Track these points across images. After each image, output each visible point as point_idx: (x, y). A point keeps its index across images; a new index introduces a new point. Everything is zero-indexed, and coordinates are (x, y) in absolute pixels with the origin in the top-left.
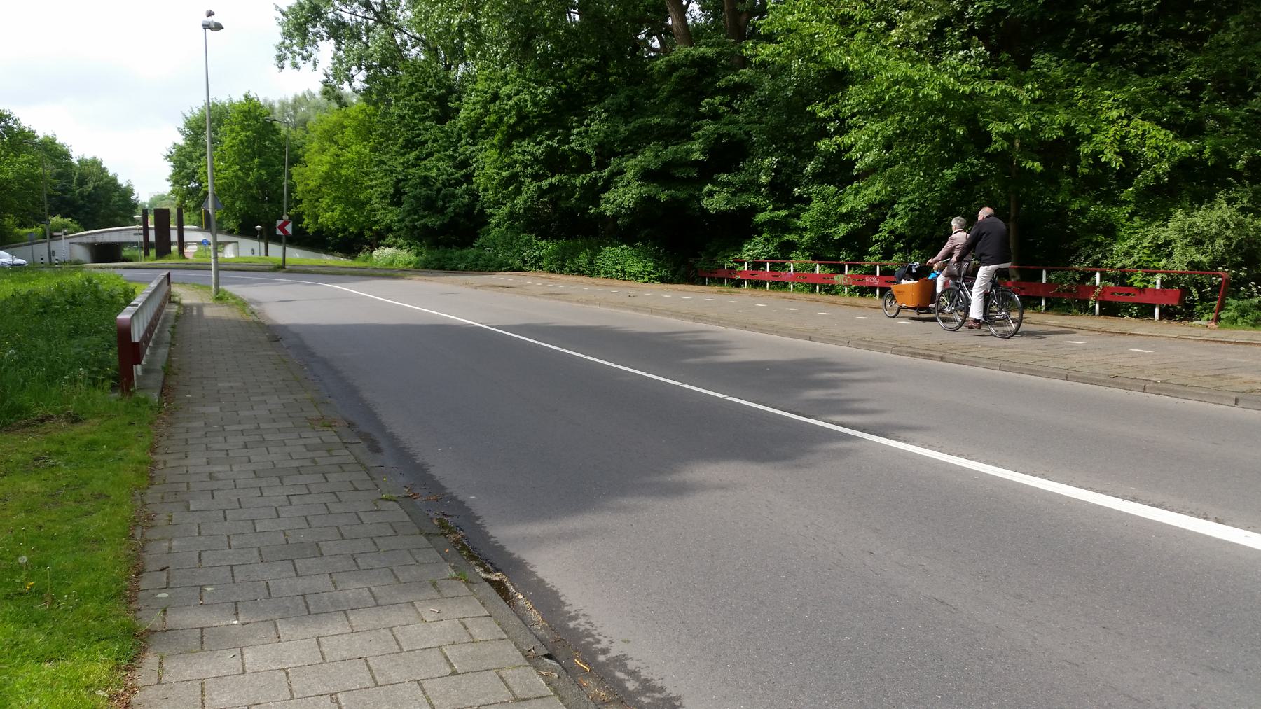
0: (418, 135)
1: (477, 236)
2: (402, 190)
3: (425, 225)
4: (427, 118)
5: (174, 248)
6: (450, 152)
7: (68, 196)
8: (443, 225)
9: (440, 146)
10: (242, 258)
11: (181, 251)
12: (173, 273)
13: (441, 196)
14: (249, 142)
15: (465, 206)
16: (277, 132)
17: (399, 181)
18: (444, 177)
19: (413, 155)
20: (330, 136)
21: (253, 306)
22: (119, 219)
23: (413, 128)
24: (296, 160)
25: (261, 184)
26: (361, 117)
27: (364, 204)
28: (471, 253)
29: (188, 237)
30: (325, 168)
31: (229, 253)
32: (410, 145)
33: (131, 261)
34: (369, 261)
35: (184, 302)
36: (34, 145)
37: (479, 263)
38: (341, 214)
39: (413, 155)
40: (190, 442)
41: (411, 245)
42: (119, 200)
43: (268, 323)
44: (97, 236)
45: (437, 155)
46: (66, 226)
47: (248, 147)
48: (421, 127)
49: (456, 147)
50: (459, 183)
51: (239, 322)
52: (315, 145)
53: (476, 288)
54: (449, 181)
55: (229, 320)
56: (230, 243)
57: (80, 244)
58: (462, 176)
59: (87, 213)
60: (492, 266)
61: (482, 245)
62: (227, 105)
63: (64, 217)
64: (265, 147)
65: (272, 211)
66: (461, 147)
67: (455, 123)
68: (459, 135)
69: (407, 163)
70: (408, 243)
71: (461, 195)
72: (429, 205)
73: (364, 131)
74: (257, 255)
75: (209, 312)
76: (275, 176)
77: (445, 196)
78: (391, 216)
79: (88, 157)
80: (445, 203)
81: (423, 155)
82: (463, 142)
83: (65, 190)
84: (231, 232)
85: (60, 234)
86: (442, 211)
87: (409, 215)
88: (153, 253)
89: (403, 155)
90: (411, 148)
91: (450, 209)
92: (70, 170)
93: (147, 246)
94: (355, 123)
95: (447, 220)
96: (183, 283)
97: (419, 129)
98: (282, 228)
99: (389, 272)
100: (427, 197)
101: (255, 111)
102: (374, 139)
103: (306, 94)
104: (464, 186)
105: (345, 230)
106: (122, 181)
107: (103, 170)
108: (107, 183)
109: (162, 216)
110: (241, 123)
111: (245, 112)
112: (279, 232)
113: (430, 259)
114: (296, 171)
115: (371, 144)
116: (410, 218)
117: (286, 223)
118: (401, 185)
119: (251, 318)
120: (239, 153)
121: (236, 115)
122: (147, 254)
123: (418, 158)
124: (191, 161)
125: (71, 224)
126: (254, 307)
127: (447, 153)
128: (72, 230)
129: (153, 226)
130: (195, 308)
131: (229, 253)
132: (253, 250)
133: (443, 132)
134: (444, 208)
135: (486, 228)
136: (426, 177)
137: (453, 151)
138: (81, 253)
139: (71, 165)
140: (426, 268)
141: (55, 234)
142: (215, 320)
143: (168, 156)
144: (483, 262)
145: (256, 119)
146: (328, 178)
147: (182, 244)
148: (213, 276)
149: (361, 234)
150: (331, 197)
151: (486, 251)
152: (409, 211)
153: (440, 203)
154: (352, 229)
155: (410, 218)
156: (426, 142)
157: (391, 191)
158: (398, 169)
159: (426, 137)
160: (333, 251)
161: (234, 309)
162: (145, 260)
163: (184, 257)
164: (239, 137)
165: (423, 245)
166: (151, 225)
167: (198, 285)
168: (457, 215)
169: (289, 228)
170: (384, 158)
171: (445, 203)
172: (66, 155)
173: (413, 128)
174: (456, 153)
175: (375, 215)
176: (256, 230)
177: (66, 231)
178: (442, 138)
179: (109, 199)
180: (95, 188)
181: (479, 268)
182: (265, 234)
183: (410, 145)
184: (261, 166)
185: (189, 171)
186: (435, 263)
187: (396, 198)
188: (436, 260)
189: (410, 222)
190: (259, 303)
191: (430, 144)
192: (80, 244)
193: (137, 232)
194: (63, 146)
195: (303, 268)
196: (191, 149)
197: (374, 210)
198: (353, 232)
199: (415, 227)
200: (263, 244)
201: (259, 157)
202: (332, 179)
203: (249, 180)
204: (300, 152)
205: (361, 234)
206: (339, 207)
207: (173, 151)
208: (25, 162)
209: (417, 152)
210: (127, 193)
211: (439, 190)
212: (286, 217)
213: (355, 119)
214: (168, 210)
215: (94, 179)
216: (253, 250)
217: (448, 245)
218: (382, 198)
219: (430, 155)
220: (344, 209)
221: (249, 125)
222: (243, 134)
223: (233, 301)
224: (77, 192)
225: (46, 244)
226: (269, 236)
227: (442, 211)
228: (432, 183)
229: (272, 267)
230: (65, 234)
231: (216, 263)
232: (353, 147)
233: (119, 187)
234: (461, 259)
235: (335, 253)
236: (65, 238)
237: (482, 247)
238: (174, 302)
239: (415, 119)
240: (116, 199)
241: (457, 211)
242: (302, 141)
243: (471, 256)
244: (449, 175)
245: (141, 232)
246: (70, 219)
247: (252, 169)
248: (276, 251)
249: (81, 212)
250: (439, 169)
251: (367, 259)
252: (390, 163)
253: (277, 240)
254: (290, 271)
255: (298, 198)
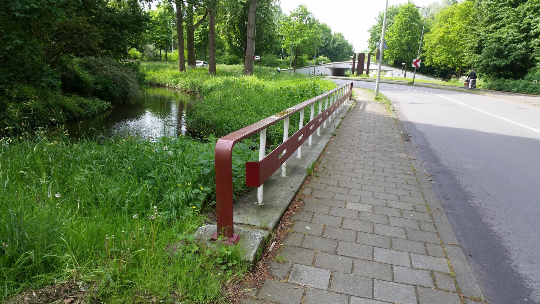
0: (497, 15)
1: (526, 73)
2: (483, 46)
3: (495, 65)
4: (505, 5)
5: (365, 72)
6: (517, 23)
7: (328, 48)
8: (506, 65)
9: (511, 20)
10: (394, 77)
11: (367, 73)
12: (354, 82)
13: (507, 49)
14: (406, 23)
15: (522, 55)
16: (419, 18)
17: (482, 40)
18: (511, 38)
19: (493, 26)
20: (445, 19)
21: (395, 104)
22: (346, 58)
23: (495, 11)
24: (427, 31)
25: (408, 43)
26: (464, 7)
27: (458, 53)
28: (521, 83)
29: (371, 67)
30: (441, 34)
31: (388, 75)
32: (492, 20)
33: (348, 76)
34: (456, 83)
35: (357, 99)
36: (319, 26)
37: (527, 89)
38: (445, 58)
39: (493, 26)
40: (355, 171)
41: (481, 76)
42: (347, 50)
43: (402, 119)
44: (336, 65)
45: (507, 26)
46: (324, 60)
47: (405, 26)
48: (500, 11)
49: (522, 21)
50: (520, 41)
51: (384, 117)
52: (437, 23)
53: (535, 106)
54: (513, 40)
55: (379, 116)
56: (389, 70)
57: (329, 68)
58: (523, 37)
59: (334, 55)
60: (536, 91)
61: (530, 78)
62: (398, 6)
63: (324, 56)
64: (413, 25)
65: (411, 56)
66: (525, 20)
67: (523, 6)
68: (525, 13)
69: (488, 30)
70: (480, 75)
71: (520, 48)
72: (499, 54)
73: (465, 15)
74: (400, 76)
75: (369, 108)
76: (414, 40)
77: (510, 48)
78: (474, 59)
79: (338, 32)
80: (509, 53)
81: (498, 26)
82: (527, 17)
83: (327, 46)
84: (390, 66)
85: (321, 63)
86: (506, 57)
87: (485, 59)
88: (355, 73)
89: (486, 26)
90: (491, 23)
91: (512, 56)
92: (330, 37)
93: (353, 70)
94: (460, 11)
95: (509, 63)
96: (363, 88)
97: (499, 12)
98: (415, 63)
99: (458, 90)
100: (499, 49)
101: (412, 8)
102: (469, 19)
103: (435, 3)
104: (524, 43)
105: (445, 66)
106: (350, 43)
107: (343, 37)
108: (343, 43)
109: (362, 56)
110: (403, 14)
111: (406, 8)
112: (413, 66)
113: (494, 85)
114: (426, 36)
115: (467, 21)
116: (486, 60)
117: (418, 61)
118: (483, 42)
119: (394, 115)
120: (400, 28)
121: (402, 10)
122: (353, 73)
123: (496, 28)
124: (379, 32)
125: (327, 60)
126: (395, 105)
127: (515, 24)
128: (326, 62)
129: (357, 62)
130: (362, 104)
131: (388, 75)
132: (399, 74)
133: (515, 12)
134: (508, 55)
135: (533, 68)
136: (499, 38)
137: (520, 23)
138: (329, 72)
139: (331, 35)
140: (491, 89)
141: (320, 63)
142: (371, 115)
143: (369, 31)
144: (530, 88)
145: (411, 12)
146: (442, 41)
147: (368, 70)
148: (376, 86)
149: (454, 69)
150: (442, 49)
151: (533, 82)
152: (486, 56)
153: (506, 53)
154: (450, 66)
155: (486, 60)
156: (502, 18)
157: (476, 46)
158: (482, 34)
159: (502, 16)
160: (437, 77)
161: (384, 107)
162: (352, 76)
163: (368, 76)
164: (402, 21)
165: (489, 77)
166: (357, 61)
167: (370, 90)
168: (516, 60)
169: (419, 64)
170: (475, 28)
171: (509, 53)
172: (329, 31)
173: (495, 11)
174: (521, 24)
175: (464, 59)
176: (402, 65)
177: (324, 62)
178: (513, 16)
179: (343, 50)
180: (338, 45)
181: (526, 92)
182: (405, 67)
183: (492, 20)
184: (409, 34)
185: (377, 37)
186: (497, 87)
187: (479, 50)
188: (498, 85)
189: (486, 62)
190: (398, 103)
191: (504, 19)
192: (329, 68)
193: (350, 64)
194: (329, 27)
195: (422, 85)
196: (379, 27)
197: (464, 56)
198: (450, 67)
199: (488, 66)
200: (404, 72)
201: (409, 30)
202: (443, 40)
203: (403, 41)
204: (430, 27)
205: (454, 69)
206: (445, 54)
207: (372, 28)
208: (312, 33)
209: (495, 25)
210: (350, 48)
211: (506, 45)
212: (418, 58)
213: (460, 9)
214: (365, 54)
215: (339, 41)
216: (399, 74)
217: (507, 77)
218: (470, 49)
219: (503, 25)
220: (448, 55)
221: (407, 15)
222: (404, 19)
223: (385, 101)
224: (332, 46)
225: (313, 68)
226: (409, 68)
227: (506, 57)
228: (502, 41)
229: (407, 83)
230: (323, 63)
231: (379, 79)
232: (457, 23)
233: (348, 45)
234: (514, 86)
235: (438, 78)
236: (323, 65)
237: (530, 80)
238: (353, 99)
239: (497, 6)
240: (346, 50)
241: (517, 57)
242: (430, 23)
243: (522, 85)
244: (514, 37)
245: (352, 64)
246: (327, 57)
247: (404, 36)
248: (410, 75)
249: (332, 55)
250: (508, 33)
251: (455, 82)
252: (478, 31)
253: (411, 69)
254: (416, 85)
255: (424, 49)
